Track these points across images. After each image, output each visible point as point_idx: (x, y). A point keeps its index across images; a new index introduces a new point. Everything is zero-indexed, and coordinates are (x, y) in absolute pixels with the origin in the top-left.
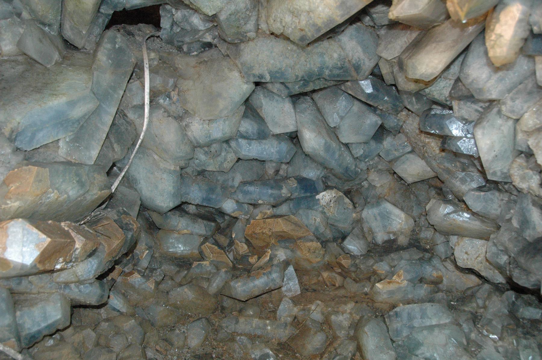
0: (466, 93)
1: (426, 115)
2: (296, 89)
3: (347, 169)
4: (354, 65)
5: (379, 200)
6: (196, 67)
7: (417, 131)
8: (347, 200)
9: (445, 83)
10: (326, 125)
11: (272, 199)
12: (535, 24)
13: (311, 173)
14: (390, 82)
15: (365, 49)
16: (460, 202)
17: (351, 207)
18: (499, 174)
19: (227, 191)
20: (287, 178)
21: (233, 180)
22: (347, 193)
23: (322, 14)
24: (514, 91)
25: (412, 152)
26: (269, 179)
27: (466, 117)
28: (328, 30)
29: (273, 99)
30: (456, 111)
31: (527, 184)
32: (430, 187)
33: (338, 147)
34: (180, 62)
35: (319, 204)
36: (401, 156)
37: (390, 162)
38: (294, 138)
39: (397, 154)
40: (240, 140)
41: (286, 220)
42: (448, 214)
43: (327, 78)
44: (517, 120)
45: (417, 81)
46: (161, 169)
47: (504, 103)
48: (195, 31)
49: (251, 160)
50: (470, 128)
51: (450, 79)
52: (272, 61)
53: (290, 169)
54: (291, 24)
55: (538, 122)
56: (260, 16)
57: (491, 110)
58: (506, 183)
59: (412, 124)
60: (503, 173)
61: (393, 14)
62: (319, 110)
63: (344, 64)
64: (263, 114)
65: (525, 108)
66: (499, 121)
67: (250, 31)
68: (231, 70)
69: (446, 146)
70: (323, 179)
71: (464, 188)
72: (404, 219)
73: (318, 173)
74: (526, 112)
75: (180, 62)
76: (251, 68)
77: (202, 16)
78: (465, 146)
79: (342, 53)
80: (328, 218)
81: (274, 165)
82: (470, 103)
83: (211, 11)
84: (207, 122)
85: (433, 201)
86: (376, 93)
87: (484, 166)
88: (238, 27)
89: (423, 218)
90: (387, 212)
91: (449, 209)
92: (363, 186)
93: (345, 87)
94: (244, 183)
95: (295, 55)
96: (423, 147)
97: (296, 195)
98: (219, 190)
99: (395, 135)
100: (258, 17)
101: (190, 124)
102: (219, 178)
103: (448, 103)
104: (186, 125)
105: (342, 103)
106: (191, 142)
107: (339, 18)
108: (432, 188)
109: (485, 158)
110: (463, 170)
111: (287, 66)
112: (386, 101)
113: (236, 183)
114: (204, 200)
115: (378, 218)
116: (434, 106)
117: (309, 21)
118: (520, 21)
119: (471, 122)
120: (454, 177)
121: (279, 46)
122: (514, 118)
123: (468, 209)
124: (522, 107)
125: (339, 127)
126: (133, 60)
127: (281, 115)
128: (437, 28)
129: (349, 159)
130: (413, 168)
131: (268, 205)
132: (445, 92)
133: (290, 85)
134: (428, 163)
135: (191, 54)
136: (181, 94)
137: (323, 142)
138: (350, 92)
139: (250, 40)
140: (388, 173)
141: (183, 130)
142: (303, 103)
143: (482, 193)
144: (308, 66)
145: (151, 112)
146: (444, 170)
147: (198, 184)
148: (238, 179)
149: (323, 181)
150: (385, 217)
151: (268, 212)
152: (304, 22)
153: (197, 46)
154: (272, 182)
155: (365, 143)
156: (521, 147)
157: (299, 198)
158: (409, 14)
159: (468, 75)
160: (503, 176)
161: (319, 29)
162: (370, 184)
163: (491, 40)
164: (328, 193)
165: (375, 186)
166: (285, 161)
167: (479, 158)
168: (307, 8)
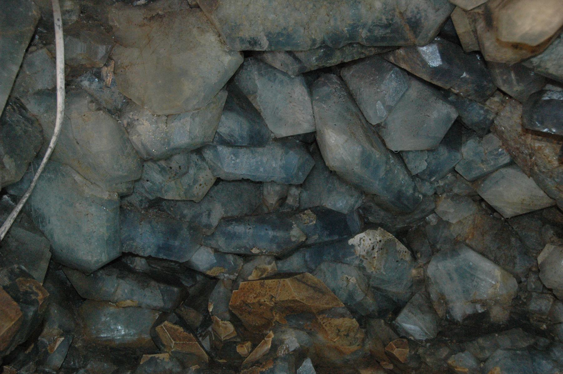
2: (313, 62)
3: (399, 195)
5: (456, 245)
6: (144, 25)
7: (520, 129)
8: (401, 247)
10: (363, 121)
11: (274, 247)
13: (340, 202)
14: (470, 47)
17: (408, 258)
19: (199, 234)
20: (299, 210)
21: (209, 215)
22: (402, 235)
25: (511, 164)
26: (269, 213)
29: (275, 79)
32: (544, 225)
33: (384, 159)
35: (353, 254)
37: (474, 181)
38: (310, 143)
39: (485, 168)
40: (220, 148)
43: (365, 43)
45: (516, 46)
46: (86, 199)
52: (271, 16)
53: (305, 195)
59: (510, 118)
62: (351, 97)
63: (392, 20)
68: (202, 31)
72: (499, 279)
73: (352, 201)
80: (369, 277)
81: (278, 188)
84: (164, 118)
85: (548, 249)
86: (446, 67)
89: (533, 278)
90: (470, 267)
92: (427, 223)
93: (394, 57)
94: (227, 220)
96: (531, 155)
98: (185, 232)
99: (481, 137)
101: (136, 123)
102: (185, 212)
104: (128, 124)
105: (391, 84)
106: (137, 152)
111: (296, 23)
112: (465, 80)
113: (215, 220)
114: (160, 249)
115: (455, 276)
125: (386, 124)
126: (35, 13)
127: (288, 106)
129: (402, 177)
131: (268, 256)
133: (301, 56)
134: (540, 183)
135: (135, 4)
137: (359, 149)
138: (404, 66)
140: (470, 200)
142: (324, 84)
144: (332, 23)
147: (150, 222)
148: (218, 212)
149: (360, 215)
150: (467, 274)
151: (269, 267)
155: (430, 151)
162: (440, 220)
164: (368, 235)
165: (447, 224)
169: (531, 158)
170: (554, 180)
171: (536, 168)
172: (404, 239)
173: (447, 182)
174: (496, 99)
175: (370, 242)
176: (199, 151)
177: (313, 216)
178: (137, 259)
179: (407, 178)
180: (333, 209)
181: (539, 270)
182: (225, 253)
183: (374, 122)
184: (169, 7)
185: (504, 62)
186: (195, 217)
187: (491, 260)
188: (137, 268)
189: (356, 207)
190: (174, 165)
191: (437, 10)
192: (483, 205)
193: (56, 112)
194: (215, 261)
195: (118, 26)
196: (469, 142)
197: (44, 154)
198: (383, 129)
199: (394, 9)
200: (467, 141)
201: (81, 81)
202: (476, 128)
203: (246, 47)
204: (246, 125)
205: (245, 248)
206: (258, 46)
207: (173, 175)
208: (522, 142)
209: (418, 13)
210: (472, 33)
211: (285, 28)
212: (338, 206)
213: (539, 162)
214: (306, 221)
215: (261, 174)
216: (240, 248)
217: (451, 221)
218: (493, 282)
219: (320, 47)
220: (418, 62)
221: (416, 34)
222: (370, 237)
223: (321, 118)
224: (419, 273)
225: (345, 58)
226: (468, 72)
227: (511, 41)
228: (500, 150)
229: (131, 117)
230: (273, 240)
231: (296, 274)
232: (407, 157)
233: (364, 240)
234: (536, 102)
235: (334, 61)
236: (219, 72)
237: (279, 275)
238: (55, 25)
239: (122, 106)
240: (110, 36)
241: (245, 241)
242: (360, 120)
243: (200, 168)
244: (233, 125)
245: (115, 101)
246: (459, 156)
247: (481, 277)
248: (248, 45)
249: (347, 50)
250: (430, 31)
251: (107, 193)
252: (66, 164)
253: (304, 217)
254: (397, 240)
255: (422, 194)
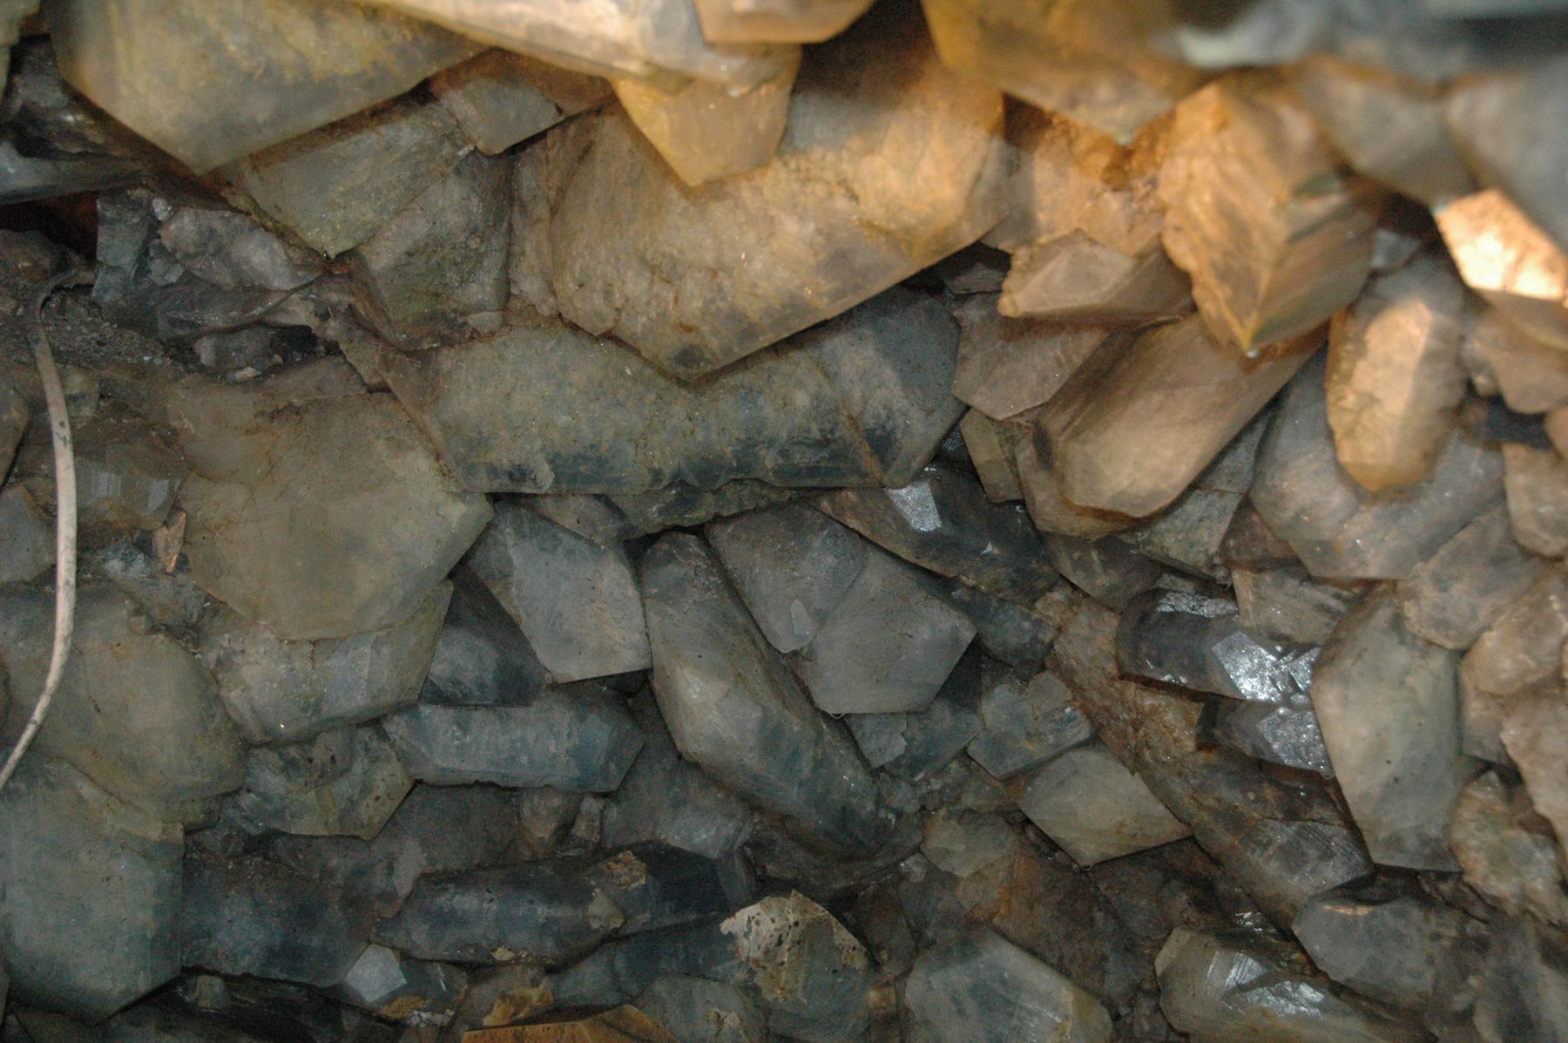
0: (1277, 551)
1: (1140, 614)
2: (653, 516)
3: (845, 816)
4: (869, 436)
5: (971, 931)
6: (257, 429)
7: (1111, 667)
9: (1204, 504)
10: (762, 645)
11: (550, 944)
12: (1481, 367)
13: (702, 831)
14: (1002, 493)
15: (911, 374)
16: (1281, 945)
17: (859, 962)
18: (1411, 843)
19: (368, 917)
20: (602, 852)
21: (390, 869)
22: (842, 905)
23: (763, 284)
24: (1442, 552)
26: (535, 861)
27: (1287, 631)
28: (786, 335)
29: (555, 548)
30: (1249, 607)
31: (1515, 880)
32: (1166, 881)
33: (812, 734)
34: (190, 408)
35: (733, 955)
36: (1055, 757)
37: (1009, 780)
38: (634, 695)
39: (1035, 750)
40: (426, 710)
41: (609, 1025)
42: (1241, 988)
43: (771, 478)
44: (1462, 653)
45: (1101, 514)
46: (106, 840)
47: (1413, 595)
48: (253, 290)
49: (458, 786)
50: (1302, 669)
51: (1222, 493)
52: (564, 420)
53: (614, 813)
54: (648, 303)
55: (1532, 664)
56: (516, 249)
57: (1370, 616)
58: (1443, 876)
59: (1090, 640)
60: (1425, 841)
61: (1014, 303)
62: (731, 587)
63: (832, 431)
64: (512, 602)
65: (1483, 614)
66: (1400, 657)
67: (481, 307)
68: (398, 447)
69: (1218, 733)
70: (748, 851)
71: (1297, 885)
72: (1071, 1011)
73: (729, 828)
74: (1489, 628)
75: (190, 408)
76: (480, 443)
77: (296, 255)
78: (1283, 741)
79: (827, 391)
80: (768, 1011)
81: (556, 802)
82: (1295, 583)
83: (334, 240)
84: (308, 648)
85: (1179, 939)
86: (949, 531)
87: (1357, 816)
88: (437, 295)
89: (1145, 1007)
90: (1004, 982)
91: (1243, 969)
92: (902, 877)
94: (434, 880)
95: (652, 396)
96: (1136, 725)
97: (642, 919)
98: (334, 913)
99: (1025, 680)
100: (509, 254)
101: (238, 659)
102: (334, 862)
103: (1220, 574)
104: (219, 662)
105: (820, 559)
106: (237, 728)
107: (826, 300)
108: (1174, 883)
109: (1356, 783)
110: (1291, 815)
111: (617, 435)
112: (991, 560)
113: (404, 881)
114: (271, 955)
115: (971, 1006)
116: (1167, 580)
117: (713, 301)
118: (1430, 357)
119: (1302, 649)
120: (1258, 843)
121: (588, 365)
122: (1450, 645)
123: (1312, 972)
124: (1474, 610)
125: (812, 651)
126: (15, 414)
127: (587, 612)
128: (1168, 330)
129: (850, 776)
130: (1100, 807)
131: (531, 965)
132: (1206, 538)
133: (626, 505)
134: (1155, 786)
135: (230, 377)
136: (197, 538)
137: (756, 714)
138: (853, 523)
139: (475, 336)
140: (1001, 821)
141: (208, 684)
142: (670, 558)
143: (1363, 911)
144: (700, 437)
145: (79, 615)
146: (1216, 814)
147: (251, 891)
148: (411, 862)
149: (746, 861)
151: (534, 994)
152: (697, 304)
153: (250, 343)
154: (547, 870)
155: (917, 713)
156: (1481, 746)
157: (650, 932)
158: (1069, 305)
159: (1282, 496)
160: (1427, 851)
161: (750, 332)
162: (932, 869)
163: (1344, 410)
164: (768, 908)
165: (950, 879)
166: (601, 786)
167: (1335, 782)
168: (709, 258)
169: (1136, 730)
170: (1187, 781)
171: (1147, 753)
172: (847, 915)
173: (950, 781)
174: (1057, 596)
175: (772, 927)
176: (375, 722)
177: (639, 867)
178: (203, 980)
179: (861, 777)
180: (686, 848)
181: (1158, 990)
182: (424, 960)
183: (786, 646)
184: (318, 389)
185: (1076, 534)
186: (358, 873)
187: (1052, 966)
188: (203, 1003)
189: (739, 842)
190: (319, 754)
191: (930, 413)
192: (1031, 834)
193: (51, 639)
194: (404, 981)
195: (193, 430)
196: (997, 690)
197: (18, 738)
198: (807, 663)
199: (837, 410)
200: (993, 687)
201: (104, 560)
202: (1009, 660)
203: (502, 485)
204: (491, 657)
205: (478, 947)
206: (530, 483)
207: (316, 776)
208: (1116, 695)
209: (889, 418)
210: (1006, 465)
211: (592, 446)
212: (697, 840)
213: (1154, 740)
214: (622, 880)
215: (522, 771)
216: (464, 946)
217: (957, 873)
218: (1058, 1020)
219: (670, 486)
220: (888, 519)
221: (885, 463)
222: (772, 915)
223: (665, 641)
224: (884, 998)
225: (723, 507)
226: (995, 544)
227: (1092, 505)
228: (1068, 710)
229: (225, 644)
230: (545, 928)
231: (602, 1009)
232: (861, 726)
233: (757, 923)
234: (1144, 617)
235: (699, 515)
236: (438, 541)
237: (558, 1012)
238: (55, 437)
239: (201, 617)
240: (169, 453)
241: (478, 931)
242: (754, 642)
243: (377, 759)
244: (464, 658)
245: (185, 607)
246: (975, 721)
247: (1030, 1006)
248: (506, 481)
249: (730, 492)
250: (914, 457)
251: (160, 824)
252: (60, 758)
253: (618, 868)
254: (834, 920)
255: (892, 810)
